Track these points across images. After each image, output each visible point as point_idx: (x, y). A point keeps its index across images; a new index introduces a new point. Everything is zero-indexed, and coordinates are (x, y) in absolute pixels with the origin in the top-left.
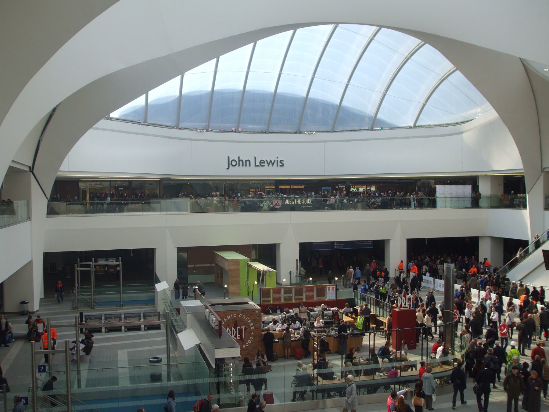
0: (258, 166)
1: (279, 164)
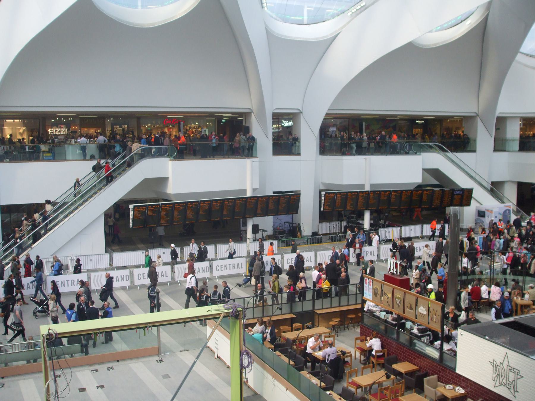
1: (141, 276)
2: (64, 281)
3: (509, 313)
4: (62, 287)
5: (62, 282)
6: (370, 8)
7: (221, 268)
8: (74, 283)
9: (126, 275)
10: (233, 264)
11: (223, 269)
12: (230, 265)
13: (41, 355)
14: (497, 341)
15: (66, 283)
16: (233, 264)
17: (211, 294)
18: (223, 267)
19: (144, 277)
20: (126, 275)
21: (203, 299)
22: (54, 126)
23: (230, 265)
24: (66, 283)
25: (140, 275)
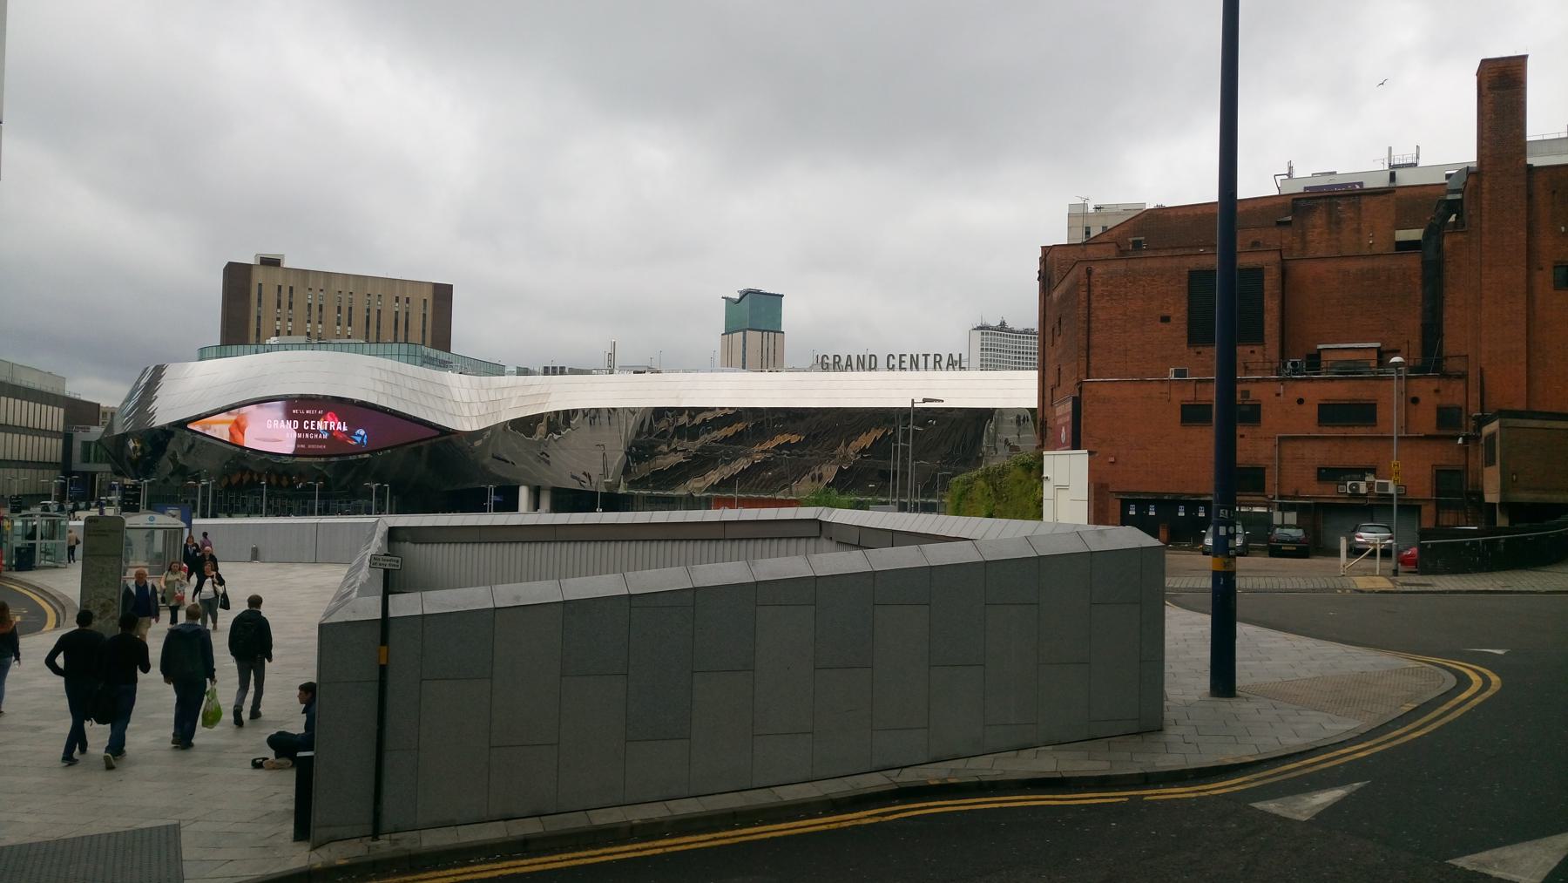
0: (905, 369)
1: (896, 362)
2: (917, 355)
3: (310, 694)
4: (917, 355)
5: (912, 356)
6: (288, 295)
7: (901, 362)
8: (941, 363)
9: (871, 356)
10: (935, 355)
11: (907, 365)
12: (926, 356)
13: (1397, 515)
14: (1132, 221)
15: (922, 359)
16: (935, 355)
17: (65, 619)
18: (907, 359)
19: (903, 366)
20: (871, 356)
21: (891, 366)
22: (1503, 686)
23: (926, 356)
24: (922, 359)
25: (894, 358)
